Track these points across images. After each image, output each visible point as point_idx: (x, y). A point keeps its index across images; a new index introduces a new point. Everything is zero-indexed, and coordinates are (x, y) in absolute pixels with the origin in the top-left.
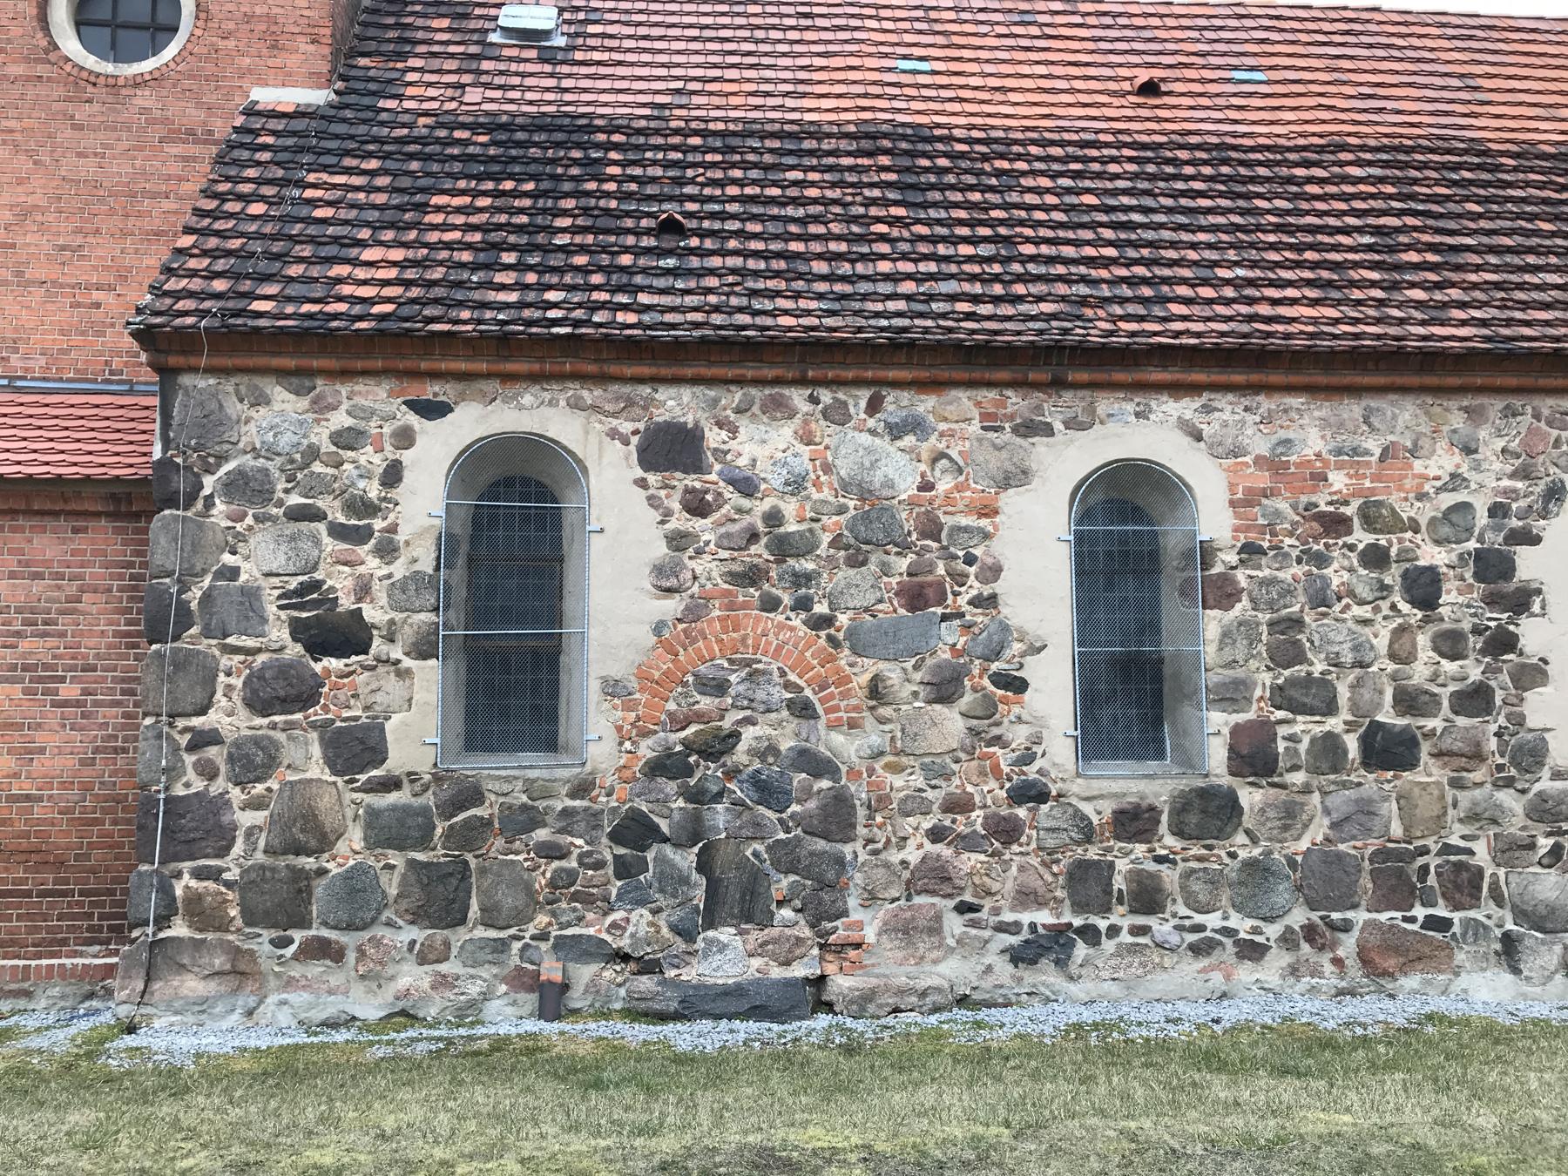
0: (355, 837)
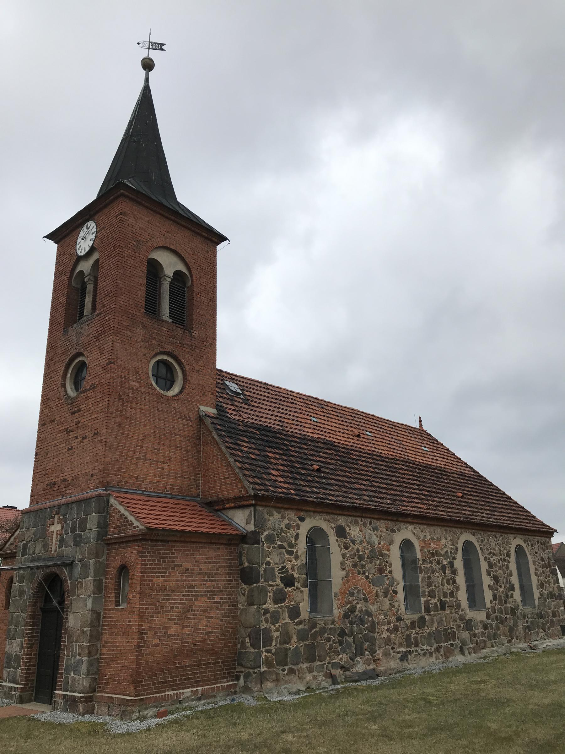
0: (294, 638)
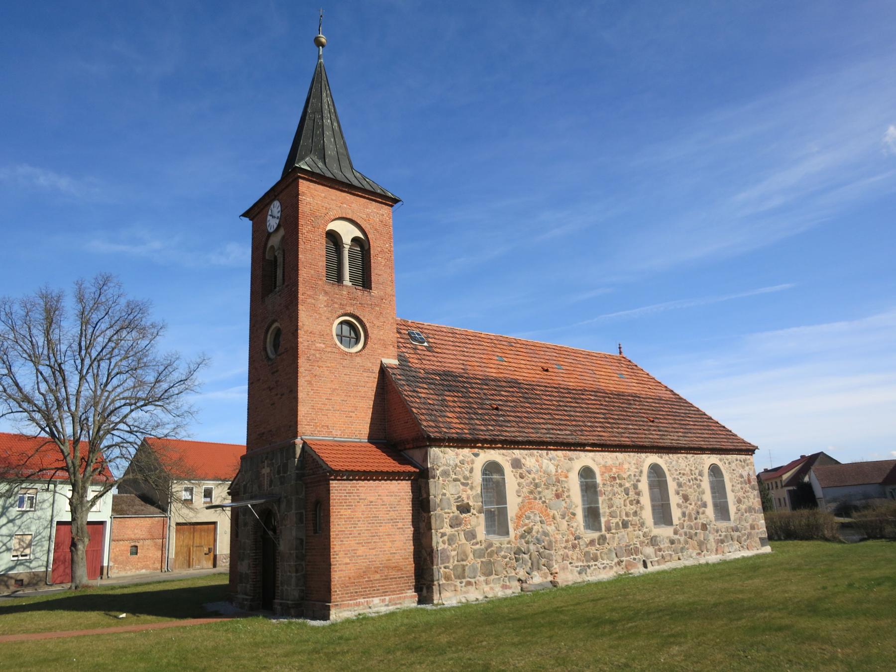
0: (471, 556)
